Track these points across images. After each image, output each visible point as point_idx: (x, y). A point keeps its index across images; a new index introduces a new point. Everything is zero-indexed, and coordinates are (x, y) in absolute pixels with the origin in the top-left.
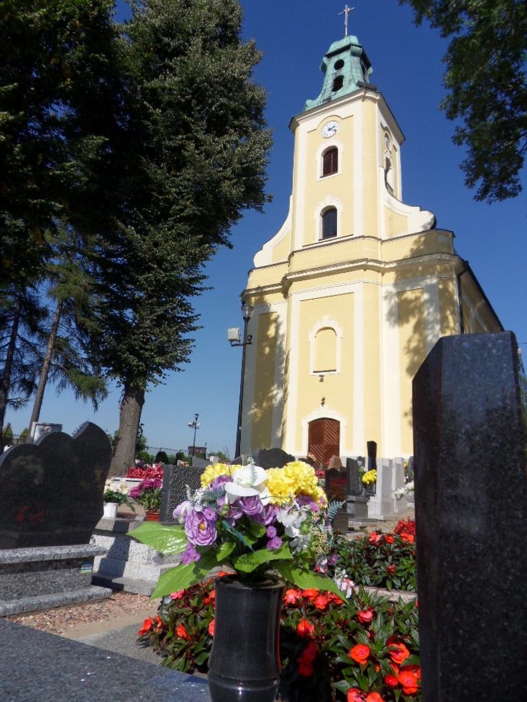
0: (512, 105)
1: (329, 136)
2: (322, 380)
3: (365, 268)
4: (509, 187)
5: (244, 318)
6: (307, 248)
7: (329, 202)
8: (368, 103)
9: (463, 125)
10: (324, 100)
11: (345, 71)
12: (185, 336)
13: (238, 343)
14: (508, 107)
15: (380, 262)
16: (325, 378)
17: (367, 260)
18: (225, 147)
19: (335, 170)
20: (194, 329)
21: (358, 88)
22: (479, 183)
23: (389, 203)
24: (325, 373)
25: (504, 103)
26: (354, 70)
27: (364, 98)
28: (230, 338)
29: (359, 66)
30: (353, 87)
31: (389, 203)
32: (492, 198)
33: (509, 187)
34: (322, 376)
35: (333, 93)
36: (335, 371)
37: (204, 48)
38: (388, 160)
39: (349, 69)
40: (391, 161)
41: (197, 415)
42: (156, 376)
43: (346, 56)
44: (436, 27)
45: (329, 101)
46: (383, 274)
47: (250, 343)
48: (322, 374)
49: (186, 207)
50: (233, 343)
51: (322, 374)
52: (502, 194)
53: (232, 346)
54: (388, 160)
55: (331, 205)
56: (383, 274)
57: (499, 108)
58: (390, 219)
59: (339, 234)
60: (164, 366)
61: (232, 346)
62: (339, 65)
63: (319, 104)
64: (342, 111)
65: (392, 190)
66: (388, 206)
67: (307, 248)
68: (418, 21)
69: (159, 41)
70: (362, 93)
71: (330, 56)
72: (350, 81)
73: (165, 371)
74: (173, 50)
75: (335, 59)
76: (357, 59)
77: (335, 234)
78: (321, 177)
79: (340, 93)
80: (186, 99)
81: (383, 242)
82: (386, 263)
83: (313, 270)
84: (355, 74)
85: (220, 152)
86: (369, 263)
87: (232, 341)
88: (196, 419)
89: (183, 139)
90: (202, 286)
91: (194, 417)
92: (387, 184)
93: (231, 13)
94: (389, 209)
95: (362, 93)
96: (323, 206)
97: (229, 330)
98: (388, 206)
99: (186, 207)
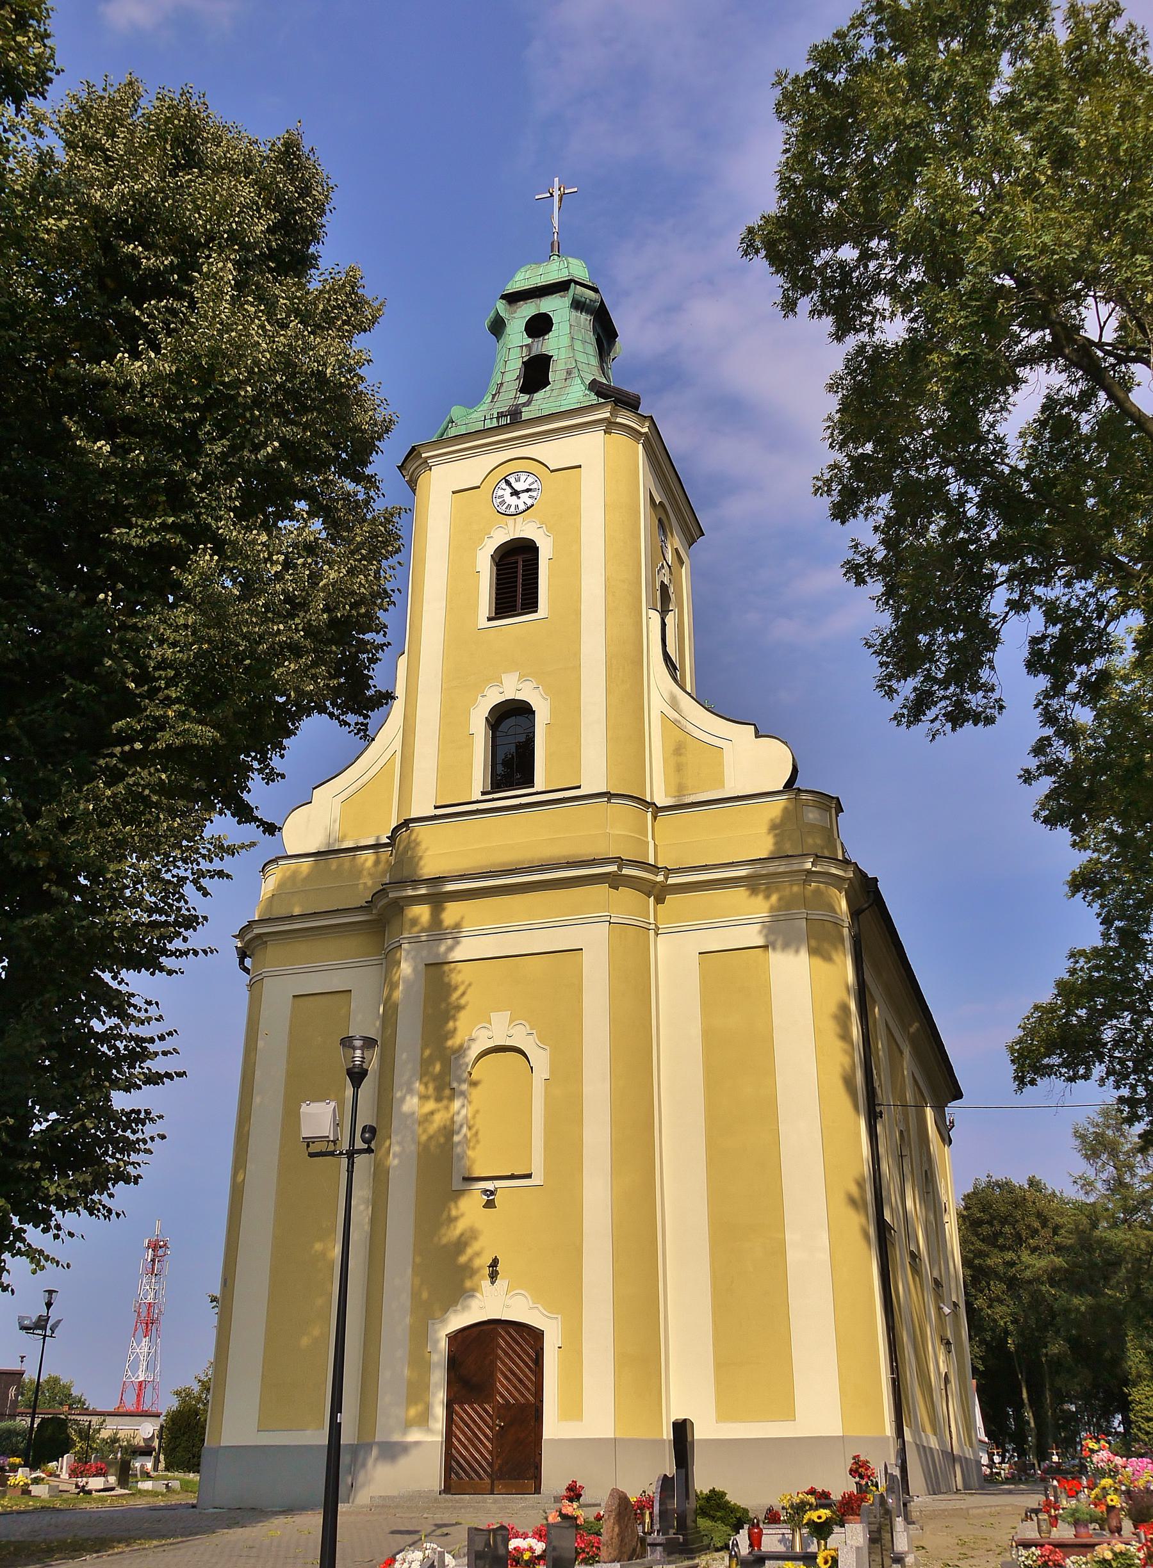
0: (979, 506)
1: (512, 510)
2: (490, 1204)
3: (615, 881)
4: (975, 700)
5: (350, 1073)
6: (446, 814)
7: (511, 689)
8: (619, 439)
9: (872, 540)
10: (501, 415)
11: (554, 344)
12: (120, 1101)
13: (331, 1148)
14: (972, 511)
15: (655, 869)
16: (497, 1199)
17: (620, 862)
18: (287, 565)
19: (531, 604)
20: (154, 1079)
21: (593, 398)
22: (907, 688)
23: (674, 704)
24: (498, 1184)
25: (962, 498)
26: (578, 346)
27: (610, 426)
28: (306, 1133)
29: (591, 337)
30: (576, 394)
31: (674, 704)
32: (937, 724)
33: (975, 700)
34: (492, 1193)
35: (524, 398)
36: (529, 1176)
37: (239, 286)
38: (664, 588)
39: (565, 341)
40: (671, 590)
41: (50, 1292)
42: (33, 1235)
43: (556, 307)
44: (820, 313)
45: (514, 417)
46: (660, 900)
47: (369, 1151)
48: (489, 1185)
49: (161, 724)
50: (314, 1148)
51: (489, 1185)
52: (959, 716)
53: (311, 1155)
54: (664, 588)
55: (519, 696)
56: (660, 900)
57: (954, 510)
58: (678, 751)
59: (540, 782)
60: (65, 1205)
61: (311, 1155)
62: (539, 326)
63: (488, 424)
64: (553, 452)
65: (675, 668)
66: (673, 715)
67: (446, 814)
68: (789, 306)
69: (108, 249)
70: (604, 414)
71: (514, 298)
72: (569, 372)
73: (66, 1219)
74: (143, 279)
75: (528, 310)
76: (585, 319)
77: (529, 781)
78: (489, 619)
79: (542, 402)
80: (184, 421)
81: (657, 810)
82: (668, 871)
83: (462, 877)
84: (581, 357)
85: (278, 577)
86: (625, 871)
87: (309, 1141)
88: (49, 1305)
89: (164, 526)
90: (183, 947)
91: (43, 1299)
92: (667, 657)
93: (302, 196)
94: (675, 722)
95: (604, 414)
96: (494, 697)
97: (304, 1108)
98: (673, 715)
99: (161, 724)
